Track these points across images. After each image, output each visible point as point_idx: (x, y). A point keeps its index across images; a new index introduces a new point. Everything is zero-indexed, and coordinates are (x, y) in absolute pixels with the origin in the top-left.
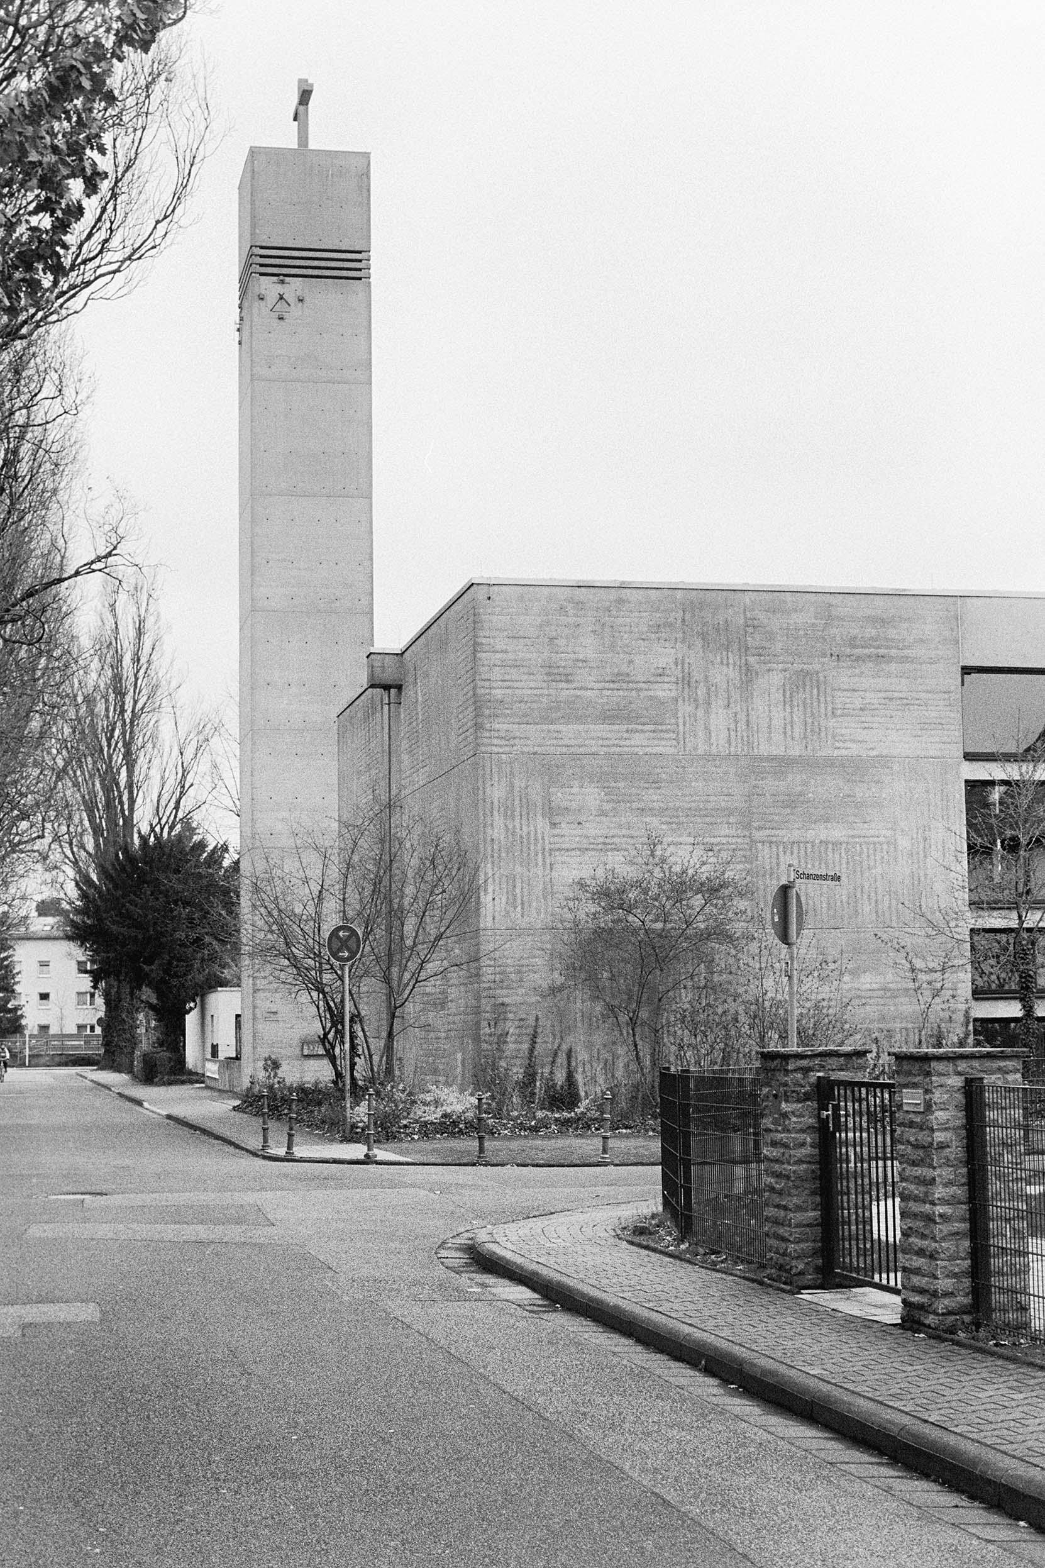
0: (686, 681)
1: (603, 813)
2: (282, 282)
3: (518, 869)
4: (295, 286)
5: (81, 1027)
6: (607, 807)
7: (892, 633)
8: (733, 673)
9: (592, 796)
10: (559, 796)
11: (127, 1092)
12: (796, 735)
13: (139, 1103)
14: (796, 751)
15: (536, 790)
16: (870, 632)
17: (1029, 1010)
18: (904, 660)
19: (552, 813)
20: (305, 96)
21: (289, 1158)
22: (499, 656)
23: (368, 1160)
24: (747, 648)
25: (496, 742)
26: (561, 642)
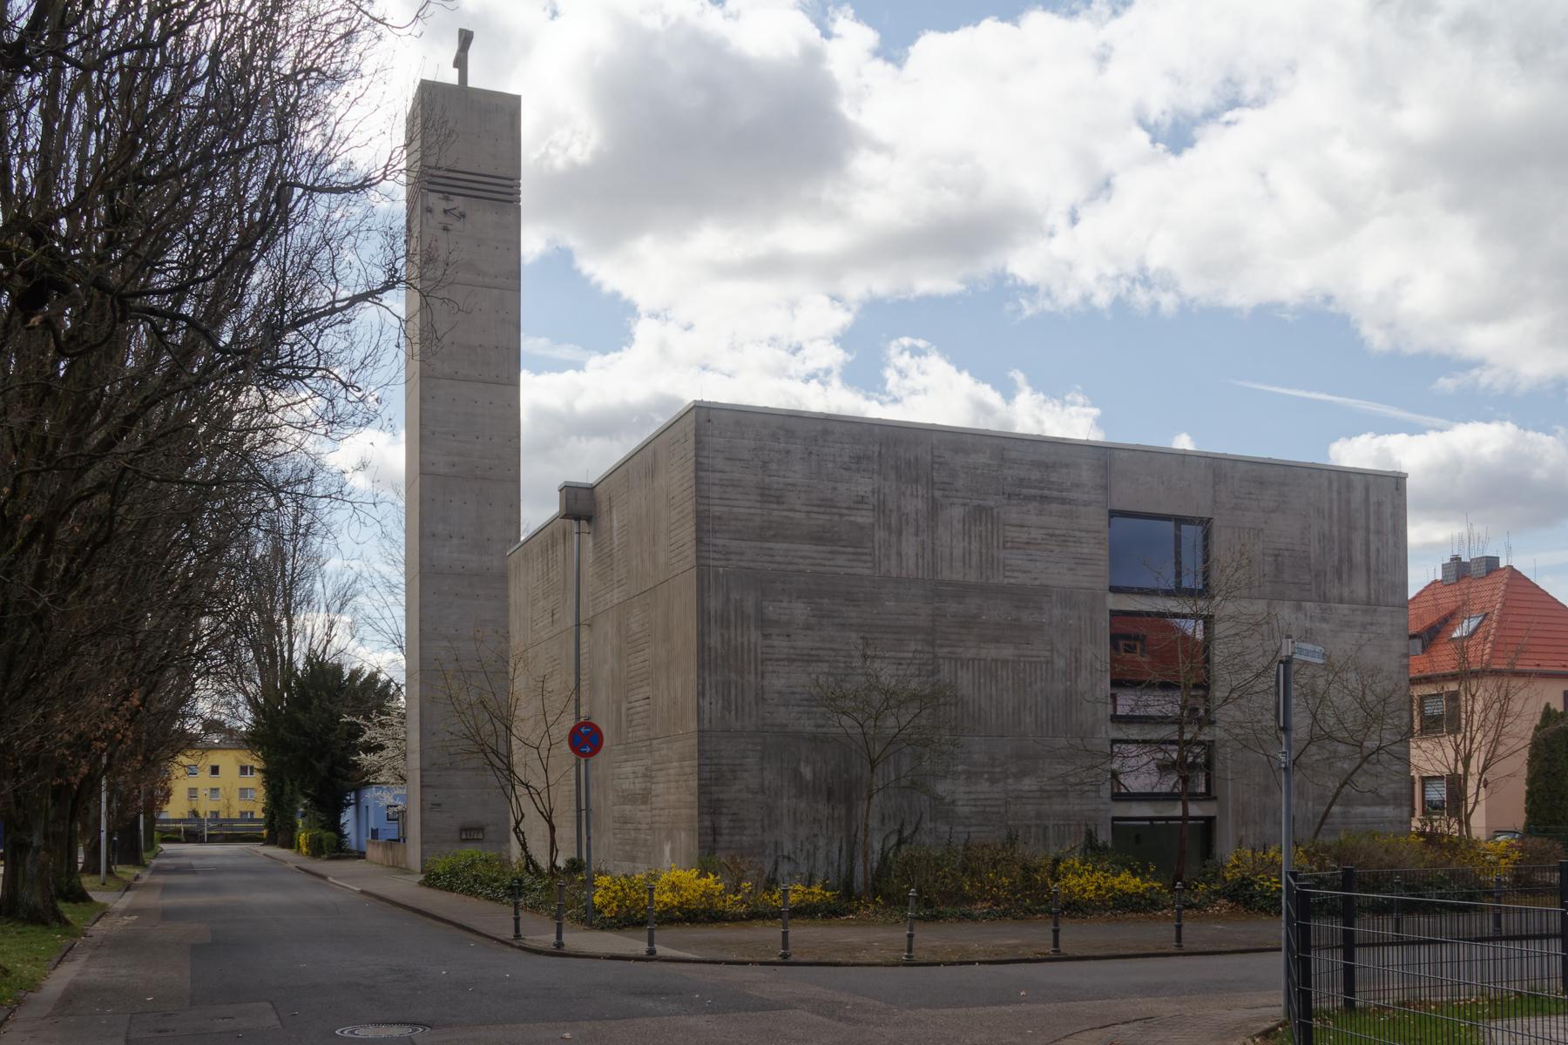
0: (881, 508)
1: (808, 627)
2: (447, 199)
3: (733, 676)
4: (458, 203)
5: (242, 813)
6: (812, 620)
7: (1054, 477)
8: (920, 504)
9: (800, 611)
10: (771, 610)
11: (305, 866)
12: (973, 563)
13: (324, 877)
14: (972, 577)
15: (749, 605)
16: (1035, 475)
17: (1185, 809)
18: (1063, 501)
19: (763, 622)
20: (466, 38)
21: (559, 951)
22: (718, 475)
23: (651, 956)
24: (933, 483)
25: (712, 555)
26: (774, 466)
